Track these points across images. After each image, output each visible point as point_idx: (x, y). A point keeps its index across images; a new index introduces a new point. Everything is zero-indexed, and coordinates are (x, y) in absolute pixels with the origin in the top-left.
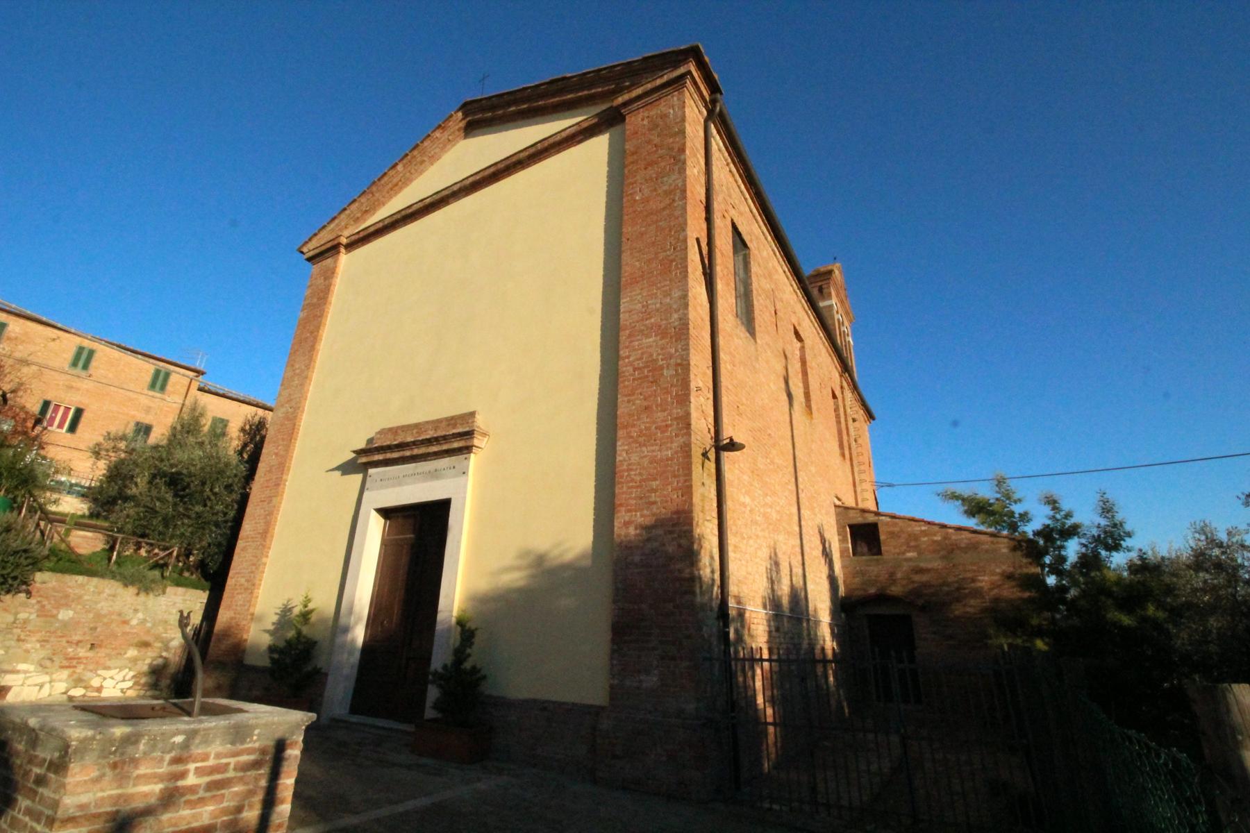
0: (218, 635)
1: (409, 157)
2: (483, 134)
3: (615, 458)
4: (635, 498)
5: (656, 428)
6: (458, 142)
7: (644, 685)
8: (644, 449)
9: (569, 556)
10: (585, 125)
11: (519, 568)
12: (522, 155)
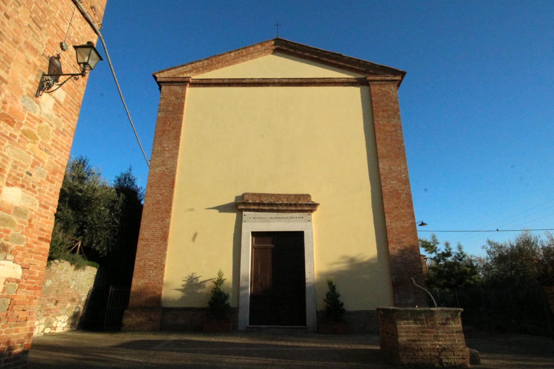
0: (133, 293)
1: (239, 51)
2: (286, 58)
3: (385, 224)
4: (396, 239)
5: (401, 215)
6: (268, 54)
7: (409, 302)
8: (397, 222)
9: (366, 259)
10: (351, 81)
11: (342, 263)
12: (317, 81)
